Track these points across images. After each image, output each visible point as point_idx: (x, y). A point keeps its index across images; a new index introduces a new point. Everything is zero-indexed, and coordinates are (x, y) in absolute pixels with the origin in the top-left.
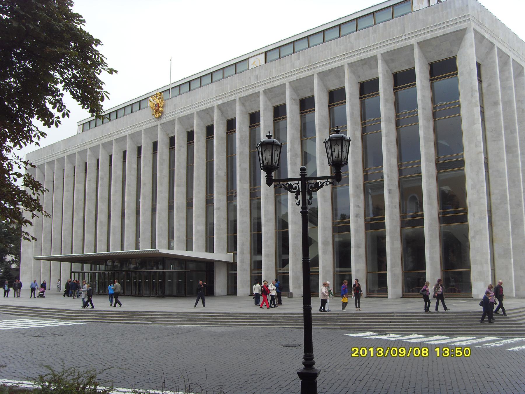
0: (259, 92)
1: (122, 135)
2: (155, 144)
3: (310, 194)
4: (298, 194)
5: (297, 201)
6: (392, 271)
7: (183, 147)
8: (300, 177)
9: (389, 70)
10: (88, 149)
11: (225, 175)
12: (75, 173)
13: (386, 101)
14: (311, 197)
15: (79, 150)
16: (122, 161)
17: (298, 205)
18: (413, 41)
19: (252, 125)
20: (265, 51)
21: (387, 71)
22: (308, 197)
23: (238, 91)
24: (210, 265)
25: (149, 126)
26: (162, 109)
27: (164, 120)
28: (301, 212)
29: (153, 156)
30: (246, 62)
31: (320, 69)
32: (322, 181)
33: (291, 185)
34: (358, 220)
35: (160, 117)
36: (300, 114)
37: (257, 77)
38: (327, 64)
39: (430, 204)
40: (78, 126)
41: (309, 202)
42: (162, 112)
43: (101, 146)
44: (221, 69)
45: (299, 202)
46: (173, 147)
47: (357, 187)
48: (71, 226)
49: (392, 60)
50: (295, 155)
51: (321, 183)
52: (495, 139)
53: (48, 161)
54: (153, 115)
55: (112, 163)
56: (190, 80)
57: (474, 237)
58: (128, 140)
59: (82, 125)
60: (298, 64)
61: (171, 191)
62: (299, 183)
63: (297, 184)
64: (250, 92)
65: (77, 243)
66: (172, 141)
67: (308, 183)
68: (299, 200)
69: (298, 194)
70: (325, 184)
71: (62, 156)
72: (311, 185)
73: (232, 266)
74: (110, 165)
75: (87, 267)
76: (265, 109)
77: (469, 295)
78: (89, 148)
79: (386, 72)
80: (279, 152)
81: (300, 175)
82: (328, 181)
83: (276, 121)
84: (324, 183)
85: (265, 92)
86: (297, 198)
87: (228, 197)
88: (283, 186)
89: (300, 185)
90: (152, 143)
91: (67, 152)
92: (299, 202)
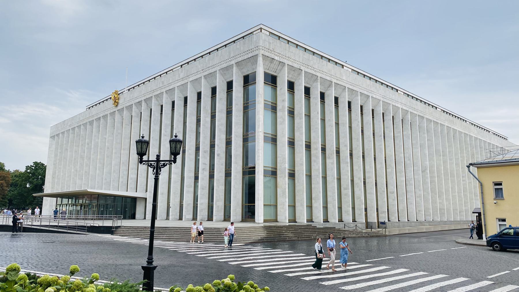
2: (199, 95)
4: (154, 169)
5: (154, 172)
7: (129, 125)
8: (156, 160)
10: (143, 101)
12: (141, 119)
16: (160, 113)
18: (233, 62)
21: (223, 81)
23: (154, 91)
24: (134, 200)
27: (119, 107)
28: (154, 178)
29: (161, 115)
31: (191, 79)
32: (167, 162)
33: (151, 164)
34: (204, 172)
35: (117, 106)
37: (163, 83)
41: (159, 173)
42: (118, 103)
43: (203, 77)
46: (215, 95)
52: (281, 123)
54: (113, 104)
58: (176, 91)
61: (213, 132)
62: (155, 163)
63: (154, 163)
64: (250, 55)
66: (214, 90)
70: (168, 164)
72: (161, 164)
74: (150, 117)
76: (166, 103)
78: (144, 100)
79: (221, 81)
80: (141, 146)
84: (167, 163)
86: (153, 171)
87: (244, 139)
89: (156, 164)
90: (184, 98)
91: (71, 127)
92: (154, 173)
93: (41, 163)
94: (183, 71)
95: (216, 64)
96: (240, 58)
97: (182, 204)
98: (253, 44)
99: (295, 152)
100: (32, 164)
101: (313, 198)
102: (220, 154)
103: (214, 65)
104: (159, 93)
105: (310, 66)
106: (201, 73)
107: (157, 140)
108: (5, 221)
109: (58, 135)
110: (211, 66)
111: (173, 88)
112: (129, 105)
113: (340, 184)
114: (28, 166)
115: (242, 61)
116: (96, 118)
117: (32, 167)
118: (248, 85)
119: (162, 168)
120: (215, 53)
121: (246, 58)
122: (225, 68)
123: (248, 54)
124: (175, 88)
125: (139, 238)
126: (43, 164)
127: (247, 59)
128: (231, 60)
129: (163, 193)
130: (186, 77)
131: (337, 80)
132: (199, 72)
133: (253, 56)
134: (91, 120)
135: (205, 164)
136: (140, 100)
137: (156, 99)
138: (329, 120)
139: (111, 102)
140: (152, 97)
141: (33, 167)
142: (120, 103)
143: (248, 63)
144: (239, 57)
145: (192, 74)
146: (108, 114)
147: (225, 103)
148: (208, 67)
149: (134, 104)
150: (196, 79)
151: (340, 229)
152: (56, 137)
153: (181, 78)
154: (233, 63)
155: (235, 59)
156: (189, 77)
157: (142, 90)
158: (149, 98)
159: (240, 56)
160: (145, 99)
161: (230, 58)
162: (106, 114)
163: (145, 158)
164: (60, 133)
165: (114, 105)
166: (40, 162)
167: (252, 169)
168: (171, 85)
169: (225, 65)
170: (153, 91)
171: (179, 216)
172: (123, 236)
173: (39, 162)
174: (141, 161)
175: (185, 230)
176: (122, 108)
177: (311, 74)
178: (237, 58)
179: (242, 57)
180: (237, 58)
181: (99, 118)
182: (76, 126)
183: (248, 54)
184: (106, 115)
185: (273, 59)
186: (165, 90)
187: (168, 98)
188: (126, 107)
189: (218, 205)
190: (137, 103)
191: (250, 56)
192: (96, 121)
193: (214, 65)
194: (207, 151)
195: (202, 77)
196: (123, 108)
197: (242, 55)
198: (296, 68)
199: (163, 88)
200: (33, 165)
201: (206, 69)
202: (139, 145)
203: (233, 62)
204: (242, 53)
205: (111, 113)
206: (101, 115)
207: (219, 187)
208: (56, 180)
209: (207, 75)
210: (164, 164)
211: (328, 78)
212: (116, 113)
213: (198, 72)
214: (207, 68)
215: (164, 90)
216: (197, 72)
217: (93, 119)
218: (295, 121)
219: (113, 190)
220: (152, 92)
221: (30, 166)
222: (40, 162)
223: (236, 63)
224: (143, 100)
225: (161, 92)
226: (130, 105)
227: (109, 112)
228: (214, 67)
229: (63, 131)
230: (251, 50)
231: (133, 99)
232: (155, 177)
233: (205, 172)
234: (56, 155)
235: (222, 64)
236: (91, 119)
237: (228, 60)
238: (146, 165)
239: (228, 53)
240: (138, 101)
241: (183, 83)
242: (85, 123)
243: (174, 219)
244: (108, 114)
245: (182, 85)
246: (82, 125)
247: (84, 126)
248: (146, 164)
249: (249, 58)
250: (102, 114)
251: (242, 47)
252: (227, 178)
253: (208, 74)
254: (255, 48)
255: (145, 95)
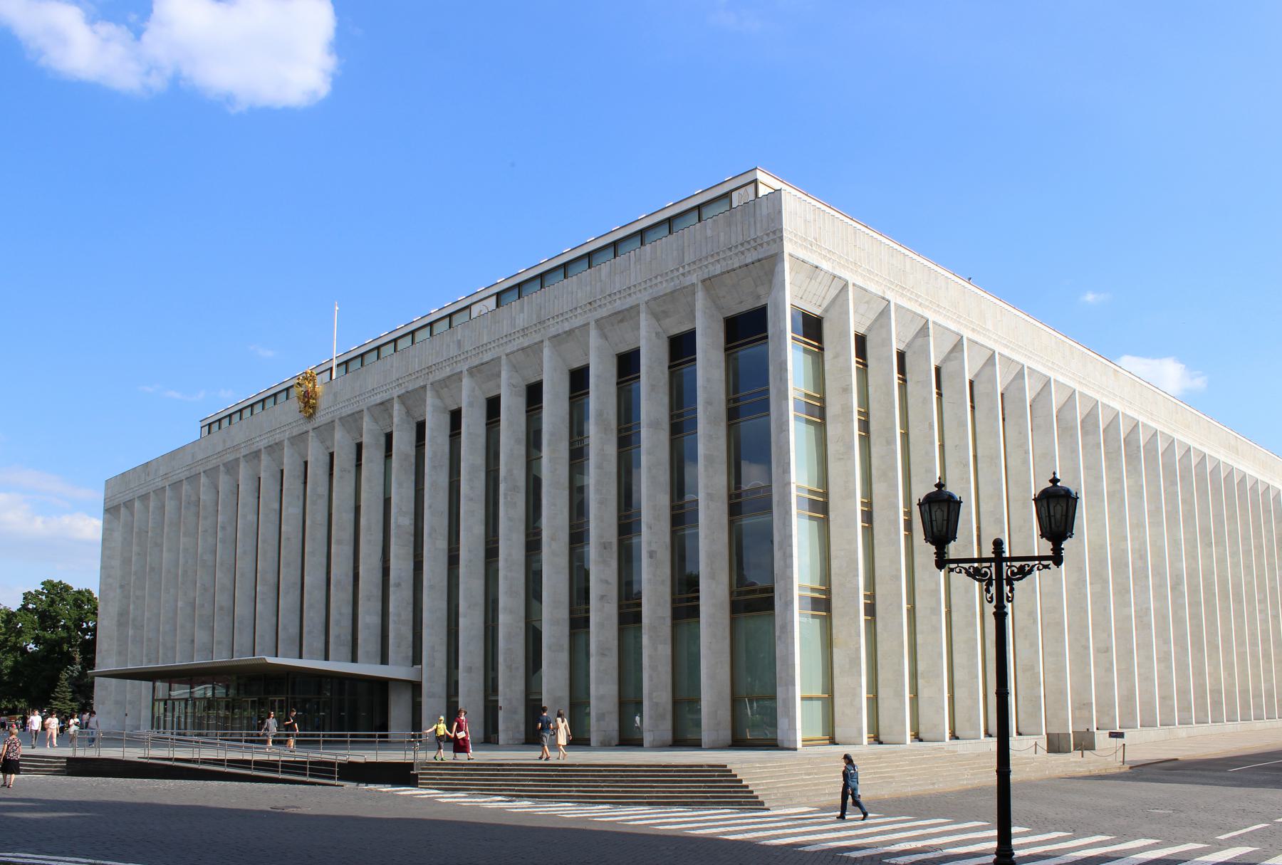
0: (462, 372)
1: (254, 448)
2: (456, 417)
3: (1010, 583)
4: (989, 584)
5: (989, 595)
6: (650, 699)
7: (349, 472)
8: (993, 556)
9: (660, 330)
11: (411, 524)
13: (653, 388)
14: (1012, 590)
15: (187, 474)
17: (990, 602)
18: (694, 278)
19: (575, 394)
20: (496, 291)
21: (657, 334)
22: (1007, 589)
24: (381, 687)
25: (296, 432)
26: (314, 401)
30: (468, 310)
31: (553, 331)
32: (1031, 563)
34: (603, 606)
35: (311, 417)
36: (527, 412)
38: (564, 321)
39: (712, 576)
40: (201, 428)
42: (314, 407)
44: (344, 362)
45: (991, 598)
46: (765, 334)
47: (605, 546)
48: (275, 618)
49: (664, 312)
50: (514, 489)
51: (1029, 566)
52: (842, 457)
53: (140, 495)
54: (300, 412)
55: (460, 427)
56: (431, 320)
57: (780, 637)
59: (207, 427)
60: (522, 320)
62: (991, 566)
63: (988, 568)
65: (242, 640)
67: (1007, 566)
68: (992, 595)
69: (989, 584)
71: (160, 485)
73: (416, 687)
75: (180, 692)
76: (471, 404)
77: (330, 736)
79: (654, 335)
80: (1046, 508)
81: (993, 553)
82: (1040, 563)
83: (574, 400)
84: (1034, 566)
85: (471, 371)
88: (963, 571)
89: (993, 569)
90: (568, 371)
91: (170, 479)
92: (991, 598)
93: (62, 584)
94: (526, 309)
95: (635, 286)
96: (718, 266)
97: (494, 698)
98: (758, 225)
99: (875, 542)
100: (40, 588)
101: (919, 672)
102: (655, 552)
103: (630, 288)
104: (448, 374)
105: (909, 290)
106: (575, 316)
107: (442, 513)
108: (147, 752)
109: (129, 504)
110: (620, 292)
111: (492, 360)
112: (349, 412)
113: (829, 637)
114: (29, 592)
115: (723, 273)
116: (244, 452)
117: (40, 597)
118: (680, 364)
119: (1014, 582)
120: (632, 252)
121: (736, 265)
122: (665, 295)
123: (742, 253)
124: (499, 358)
125: (500, 795)
126: (68, 586)
127: (740, 267)
128: (686, 271)
129: (471, 668)
130: (535, 325)
131: (973, 330)
132: (579, 311)
133: (759, 260)
134: (231, 459)
135: (607, 582)
136: (386, 396)
137: (437, 391)
138: (956, 446)
139: (294, 404)
140: (424, 387)
141: (42, 594)
142: (322, 408)
143: (743, 279)
144: (712, 263)
145: (557, 316)
146: (284, 440)
147: (666, 400)
148: (610, 295)
149: (365, 410)
150: (570, 333)
151: (726, 766)
152: (123, 510)
153: (517, 330)
154: (695, 281)
155: (700, 268)
156: (545, 325)
157: (392, 367)
158: (415, 390)
159: (718, 261)
160: (403, 395)
161: (683, 267)
162: (277, 441)
163: (953, 550)
164: (136, 497)
165: (303, 414)
166: (60, 582)
167: (760, 596)
168: (486, 351)
169: (666, 287)
170: (427, 371)
171: (523, 733)
172: (446, 790)
173: (56, 581)
174: (941, 562)
175: (624, 771)
176: (329, 423)
177: (911, 311)
178: (706, 266)
179: (724, 263)
180: (706, 266)
181: (256, 452)
182: (183, 476)
183: (742, 253)
184: (276, 444)
185: (817, 267)
186: (467, 367)
187: (477, 388)
188: (341, 419)
189: (654, 700)
190: (377, 405)
191: (750, 260)
192: (247, 462)
193: (630, 288)
194: (611, 543)
195: (589, 324)
196: (333, 421)
197: (722, 256)
198: (876, 295)
199: (460, 361)
200: (43, 589)
201: (603, 302)
202: (939, 513)
203: (694, 278)
204: (724, 251)
205: (293, 437)
206: (262, 444)
207: (656, 649)
208: (131, 632)
209: (606, 317)
210: (1021, 569)
211: (953, 327)
212: (310, 439)
213: (576, 309)
214: (605, 297)
215: (464, 367)
216: (571, 310)
217: (238, 456)
218: (873, 450)
219: (311, 658)
220: (424, 372)
221: (34, 593)
222: (60, 582)
223: (704, 281)
224: (395, 396)
225: (455, 372)
226: (353, 414)
227: (287, 434)
228: (630, 295)
229: (143, 491)
230: (752, 242)
231: (364, 397)
232: (995, 610)
233: (605, 604)
234: (127, 561)
235: (656, 285)
236: (230, 457)
237: (676, 274)
238: (960, 572)
239: (675, 253)
240: (379, 401)
241: (526, 342)
242: (210, 469)
243: (511, 742)
244: (284, 440)
245: (523, 349)
246: (202, 474)
247: (208, 477)
248: (958, 570)
249: (747, 265)
250: (267, 440)
251: (722, 234)
252: (735, 616)
253: (610, 316)
254: (768, 235)
255: (400, 381)
